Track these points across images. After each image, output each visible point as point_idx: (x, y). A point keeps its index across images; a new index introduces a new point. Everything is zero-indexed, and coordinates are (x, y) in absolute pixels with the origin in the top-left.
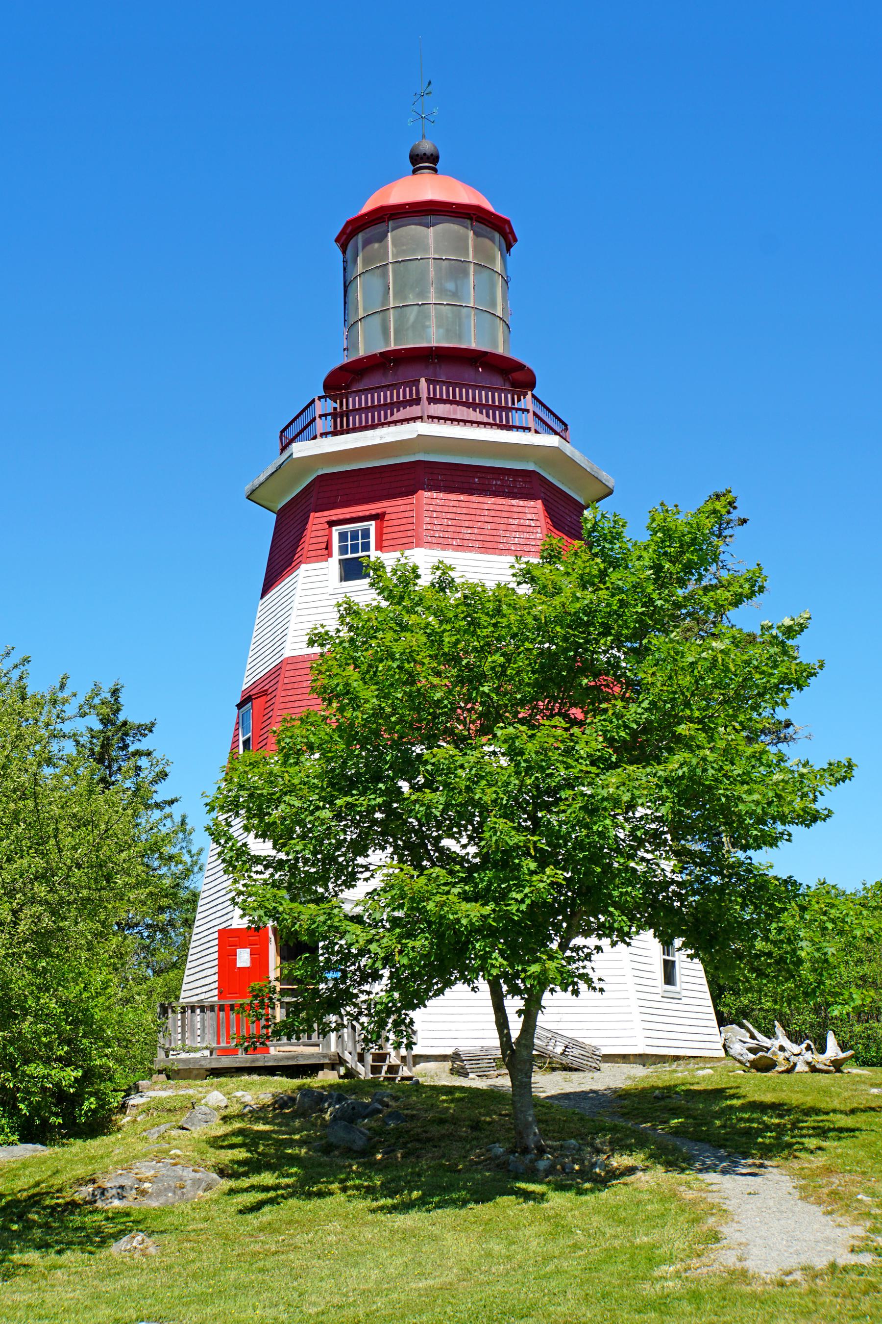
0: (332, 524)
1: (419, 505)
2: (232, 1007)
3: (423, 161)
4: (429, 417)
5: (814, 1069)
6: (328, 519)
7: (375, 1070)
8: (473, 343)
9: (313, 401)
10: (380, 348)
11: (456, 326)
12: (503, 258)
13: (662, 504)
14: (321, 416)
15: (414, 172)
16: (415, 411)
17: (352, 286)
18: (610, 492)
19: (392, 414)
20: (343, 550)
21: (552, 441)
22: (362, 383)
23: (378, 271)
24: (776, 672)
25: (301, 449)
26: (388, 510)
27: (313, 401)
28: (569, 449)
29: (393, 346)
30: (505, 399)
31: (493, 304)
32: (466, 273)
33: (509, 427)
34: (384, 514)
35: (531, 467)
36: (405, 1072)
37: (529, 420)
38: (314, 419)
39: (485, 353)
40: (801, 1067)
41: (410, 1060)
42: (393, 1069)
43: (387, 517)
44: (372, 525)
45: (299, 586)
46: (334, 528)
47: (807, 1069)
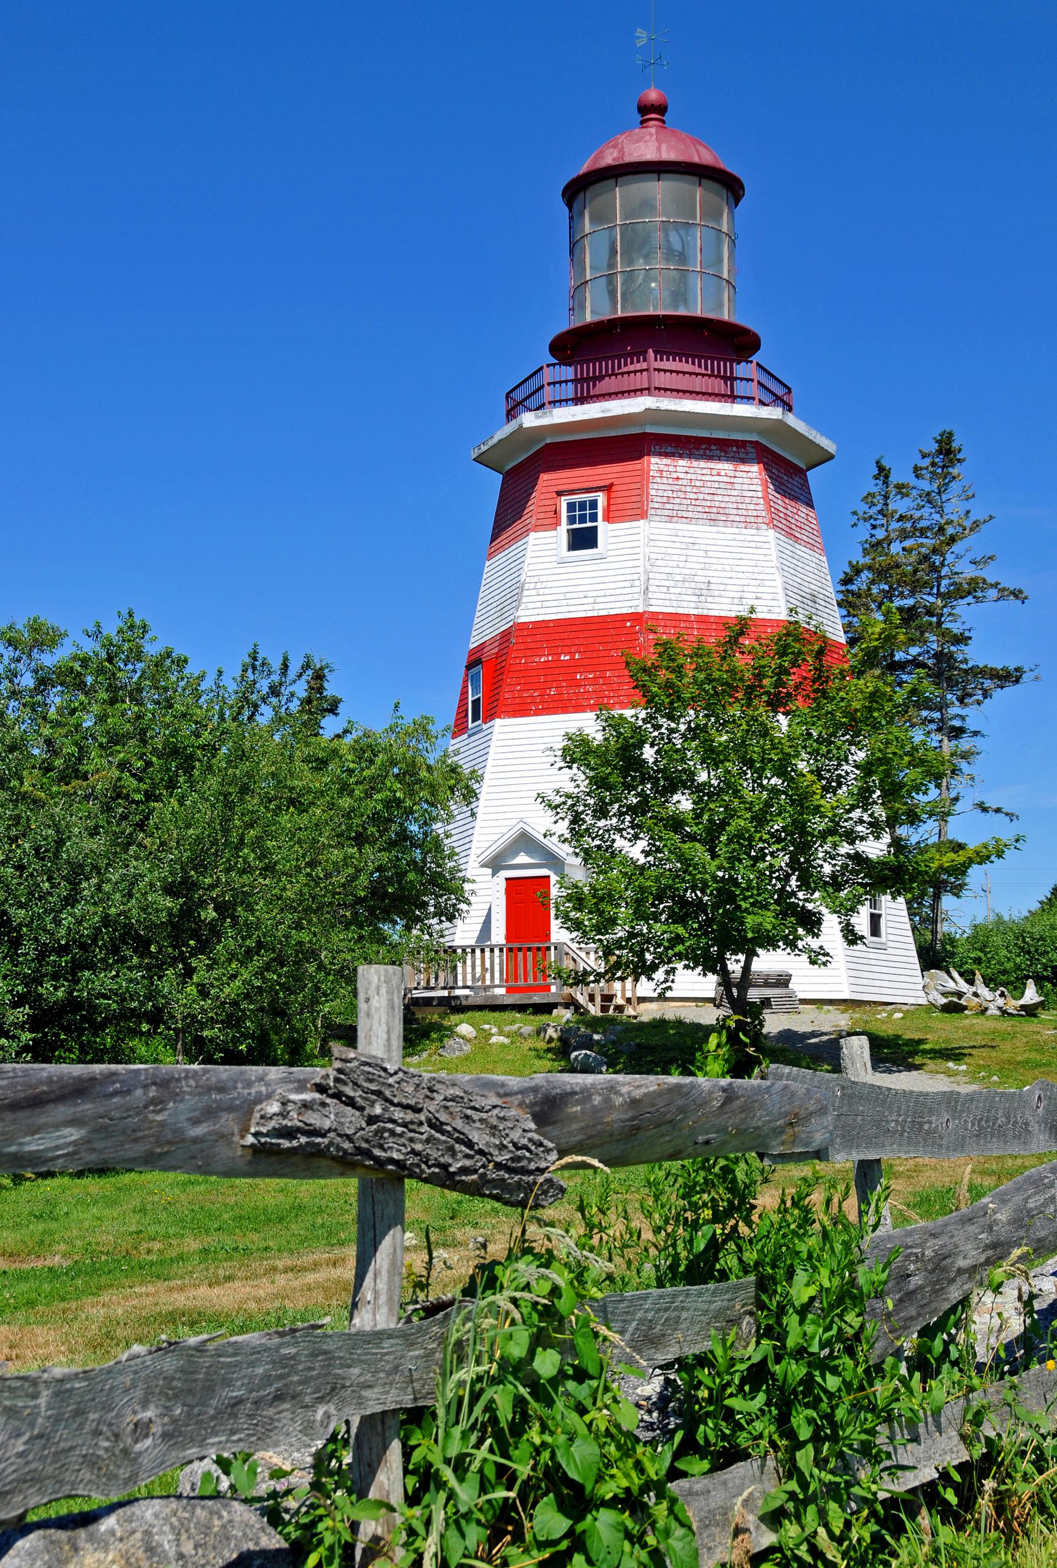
0: (560, 494)
3: (651, 111)
5: (1004, 1012)
7: (605, 1009)
8: (698, 308)
9: (542, 368)
10: (606, 315)
11: (680, 296)
12: (731, 213)
13: (855, 513)
14: (549, 384)
19: (619, 368)
20: (571, 520)
21: (774, 413)
23: (604, 279)
24: (39, 1401)
25: (529, 420)
26: (616, 482)
27: (542, 368)
28: (792, 420)
29: (620, 314)
31: (721, 270)
35: (754, 438)
36: (630, 1011)
37: (752, 389)
38: (542, 387)
39: (712, 320)
40: (993, 1011)
41: (634, 1001)
42: (619, 1009)
43: (614, 488)
44: (601, 498)
45: (530, 548)
47: (998, 1013)
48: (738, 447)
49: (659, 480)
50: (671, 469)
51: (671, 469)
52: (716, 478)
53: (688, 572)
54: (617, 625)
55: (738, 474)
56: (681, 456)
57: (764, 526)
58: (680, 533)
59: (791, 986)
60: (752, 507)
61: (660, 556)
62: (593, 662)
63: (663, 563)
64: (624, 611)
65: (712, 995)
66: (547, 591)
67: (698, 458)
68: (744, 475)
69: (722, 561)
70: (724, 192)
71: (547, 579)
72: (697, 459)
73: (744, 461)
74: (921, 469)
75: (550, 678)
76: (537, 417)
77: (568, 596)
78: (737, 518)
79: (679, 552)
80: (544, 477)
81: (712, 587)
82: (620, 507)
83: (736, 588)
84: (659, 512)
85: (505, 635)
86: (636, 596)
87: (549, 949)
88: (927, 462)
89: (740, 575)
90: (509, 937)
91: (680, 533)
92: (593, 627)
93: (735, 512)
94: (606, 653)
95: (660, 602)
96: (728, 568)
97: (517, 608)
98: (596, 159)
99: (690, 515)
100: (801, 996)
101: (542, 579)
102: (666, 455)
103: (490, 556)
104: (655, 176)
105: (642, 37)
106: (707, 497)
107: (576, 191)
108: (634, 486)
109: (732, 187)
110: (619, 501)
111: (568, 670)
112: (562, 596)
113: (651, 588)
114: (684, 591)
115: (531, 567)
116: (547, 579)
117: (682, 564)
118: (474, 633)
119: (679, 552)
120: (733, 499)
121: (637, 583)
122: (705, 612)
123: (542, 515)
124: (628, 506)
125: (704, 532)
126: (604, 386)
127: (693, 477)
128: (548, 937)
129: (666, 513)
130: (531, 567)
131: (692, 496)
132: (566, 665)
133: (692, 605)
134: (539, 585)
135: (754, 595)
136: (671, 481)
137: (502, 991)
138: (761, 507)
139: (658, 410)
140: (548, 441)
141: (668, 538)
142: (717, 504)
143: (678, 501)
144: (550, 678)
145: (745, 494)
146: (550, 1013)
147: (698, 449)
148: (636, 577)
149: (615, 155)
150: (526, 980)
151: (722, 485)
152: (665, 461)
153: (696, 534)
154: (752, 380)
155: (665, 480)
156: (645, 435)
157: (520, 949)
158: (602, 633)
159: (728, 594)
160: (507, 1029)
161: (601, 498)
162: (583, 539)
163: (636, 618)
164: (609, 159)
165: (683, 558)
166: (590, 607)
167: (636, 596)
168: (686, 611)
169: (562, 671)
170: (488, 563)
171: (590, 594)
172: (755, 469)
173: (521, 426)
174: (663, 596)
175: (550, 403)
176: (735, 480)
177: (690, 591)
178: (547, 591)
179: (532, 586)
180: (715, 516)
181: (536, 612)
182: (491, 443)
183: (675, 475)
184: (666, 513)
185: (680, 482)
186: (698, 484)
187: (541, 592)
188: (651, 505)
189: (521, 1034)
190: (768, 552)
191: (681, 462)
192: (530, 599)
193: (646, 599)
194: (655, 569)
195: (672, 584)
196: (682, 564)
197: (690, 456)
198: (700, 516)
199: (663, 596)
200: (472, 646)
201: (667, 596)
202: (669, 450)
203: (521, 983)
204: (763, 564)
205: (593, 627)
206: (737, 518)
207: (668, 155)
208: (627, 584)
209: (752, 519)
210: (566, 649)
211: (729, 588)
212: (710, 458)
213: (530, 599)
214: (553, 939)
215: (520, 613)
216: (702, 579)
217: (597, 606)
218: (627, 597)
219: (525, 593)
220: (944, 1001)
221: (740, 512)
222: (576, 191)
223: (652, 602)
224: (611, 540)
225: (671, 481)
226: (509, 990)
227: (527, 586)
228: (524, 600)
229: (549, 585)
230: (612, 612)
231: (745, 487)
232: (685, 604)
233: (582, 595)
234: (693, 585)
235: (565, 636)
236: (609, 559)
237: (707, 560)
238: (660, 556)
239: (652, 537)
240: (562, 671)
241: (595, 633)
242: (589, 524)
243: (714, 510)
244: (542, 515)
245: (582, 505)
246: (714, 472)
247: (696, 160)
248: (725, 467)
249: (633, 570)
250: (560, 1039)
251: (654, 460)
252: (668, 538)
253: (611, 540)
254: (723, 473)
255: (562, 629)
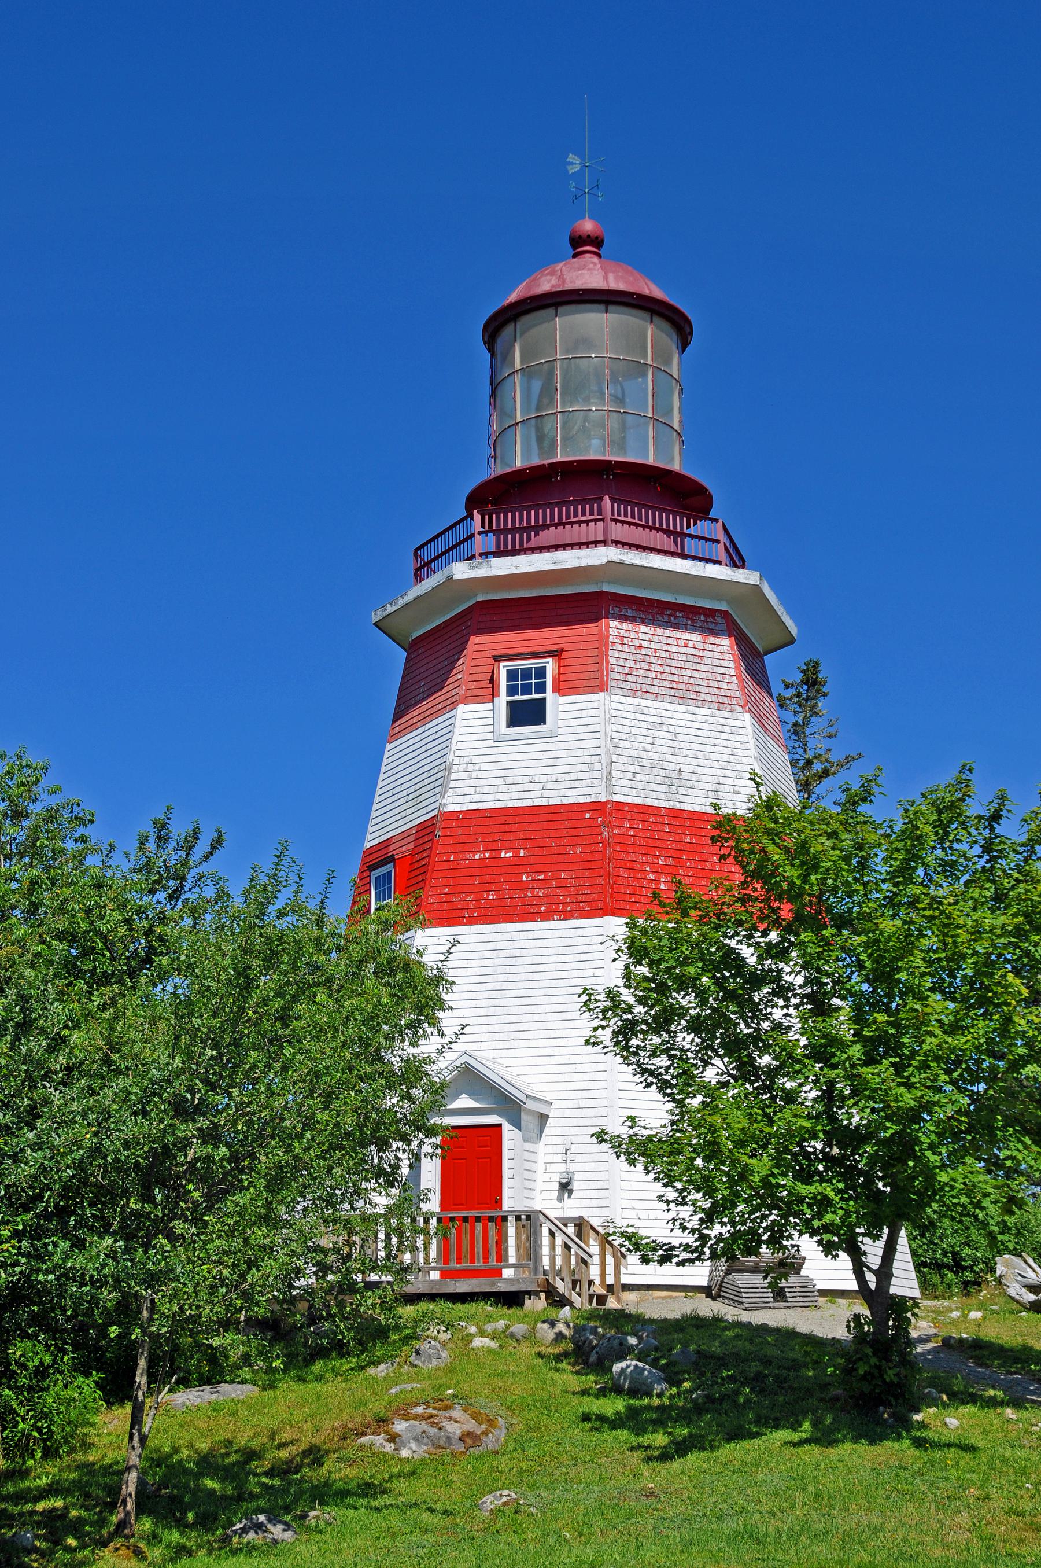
0: (498, 659)
1: (602, 646)
2: (452, 1219)
3: (579, 243)
4: (613, 542)
6: (495, 652)
10: (536, 461)
15: (575, 256)
16: (596, 531)
17: (507, 385)
18: (792, 641)
19: (529, 539)
20: (512, 690)
22: (521, 498)
26: (566, 647)
29: (560, 458)
30: (677, 522)
32: (644, 375)
33: (683, 556)
34: (562, 651)
35: (723, 607)
36: (612, 1304)
38: (473, 535)
43: (564, 655)
44: (550, 666)
45: (458, 723)
46: (502, 664)
48: (706, 616)
49: (619, 647)
50: (633, 635)
51: (633, 635)
52: (683, 650)
53: (656, 756)
54: (574, 816)
55: (707, 647)
56: (643, 622)
57: (740, 709)
58: (646, 710)
59: (803, 1272)
60: (725, 686)
61: (624, 736)
62: (543, 860)
63: (627, 744)
64: (582, 800)
65: (704, 1282)
66: (480, 774)
67: (663, 625)
68: (715, 648)
69: (693, 746)
70: (675, 336)
71: (479, 758)
72: (661, 627)
73: (713, 633)
74: (785, 699)
75: (487, 879)
76: (472, 568)
77: (509, 780)
78: (708, 698)
79: (644, 732)
80: (475, 640)
81: (684, 776)
82: (573, 677)
83: (710, 779)
84: (621, 684)
85: (426, 829)
86: (596, 782)
87: (504, 1219)
88: (790, 692)
89: (715, 764)
90: (444, 1205)
91: (646, 710)
92: (542, 818)
93: (706, 690)
94: (561, 850)
95: (626, 791)
96: (700, 755)
97: (443, 794)
98: (528, 287)
99: (656, 690)
100: (821, 1285)
101: (475, 760)
102: (627, 619)
103: (394, 737)
104: (602, 307)
105: (574, 163)
106: (674, 671)
107: (500, 324)
108: (589, 653)
109: (680, 325)
110: (570, 670)
111: (510, 870)
112: (501, 781)
113: (614, 773)
114: (652, 779)
115: (460, 746)
116: (479, 758)
117: (649, 747)
118: (370, 829)
119: (644, 732)
120: (703, 675)
121: (597, 766)
122: (678, 806)
123: (474, 685)
124: (582, 676)
125: (675, 713)
126: (549, 536)
127: (658, 646)
128: (498, 1204)
129: (629, 686)
130: (460, 746)
131: (657, 668)
132: (508, 863)
133: (662, 796)
134: (470, 767)
135: (731, 789)
136: (632, 649)
137: (435, 1275)
138: (735, 686)
139: (621, 563)
140: (480, 598)
141: (632, 716)
142: (686, 680)
143: (641, 673)
144: (487, 879)
145: (716, 670)
146: (521, 1304)
147: (662, 614)
148: (595, 759)
149: (554, 281)
150: (486, 1259)
151: (691, 658)
152: (626, 626)
153: (664, 713)
154: (718, 542)
155: (626, 648)
156: (601, 594)
157: (478, 1219)
158: (554, 825)
159: (701, 785)
160: (489, 1327)
161: (550, 666)
162: (527, 713)
163: (598, 807)
164: (546, 285)
165: (650, 740)
166: (538, 794)
167: (596, 782)
168: (655, 803)
169: (503, 870)
170: (389, 746)
171: (537, 779)
172: (726, 642)
173: (450, 578)
174: (628, 783)
175: (481, 555)
176: (706, 654)
177: (658, 780)
178: (480, 774)
179: (462, 768)
180: (684, 694)
181: (468, 798)
182: (402, 602)
183: (637, 643)
184: (629, 686)
185: (643, 651)
186: (663, 654)
187: (474, 775)
188: (612, 675)
189: (512, 1336)
190: (745, 739)
191: (644, 628)
192: (460, 784)
193: (609, 786)
194: (619, 751)
195: (638, 769)
196: (649, 747)
197: (654, 623)
198: (667, 691)
199: (628, 783)
200: (368, 845)
201: (634, 784)
202: (629, 613)
203: (479, 1264)
204: (740, 752)
205: (542, 818)
206: (708, 698)
207: (615, 283)
208: (584, 768)
209: (726, 700)
210: (507, 844)
211: (703, 778)
212: (675, 626)
213: (460, 784)
214: (507, 1205)
215: (448, 799)
216: (672, 766)
217: (546, 794)
218: (584, 783)
219: (453, 776)
220: (1032, 1297)
221: (711, 691)
222: (500, 324)
223: (617, 789)
224: (562, 716)
225: (632, 649)
226: (444, 1274)
227: (455, 768)
228: (452, 784)
229: (484, 767)
230: (566, 801)
231: (716, 662)
232: (654, 795)
233: (526, 779)
234: (662, 773)
235: (507, 828)
236: (560, 738)
237: (676, 744)
238: (624, 736)
239: (614, 713)
240: (503, 870)
241: (545, 826)
242: (534, 696)
243: (683, 686)
244: (474, 685)
245: (526, 673)
246: (681, 643)
247: (646, 292)
248: (692, 637)
249: (592, 752)
250: (573, 1339)
251: (613, 623)
252: (632, 716)
253: (562, 716)
254: (691, 644)
255: (502, 820)
